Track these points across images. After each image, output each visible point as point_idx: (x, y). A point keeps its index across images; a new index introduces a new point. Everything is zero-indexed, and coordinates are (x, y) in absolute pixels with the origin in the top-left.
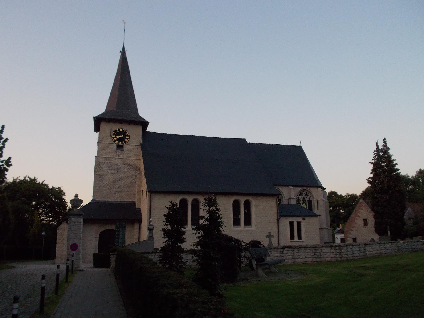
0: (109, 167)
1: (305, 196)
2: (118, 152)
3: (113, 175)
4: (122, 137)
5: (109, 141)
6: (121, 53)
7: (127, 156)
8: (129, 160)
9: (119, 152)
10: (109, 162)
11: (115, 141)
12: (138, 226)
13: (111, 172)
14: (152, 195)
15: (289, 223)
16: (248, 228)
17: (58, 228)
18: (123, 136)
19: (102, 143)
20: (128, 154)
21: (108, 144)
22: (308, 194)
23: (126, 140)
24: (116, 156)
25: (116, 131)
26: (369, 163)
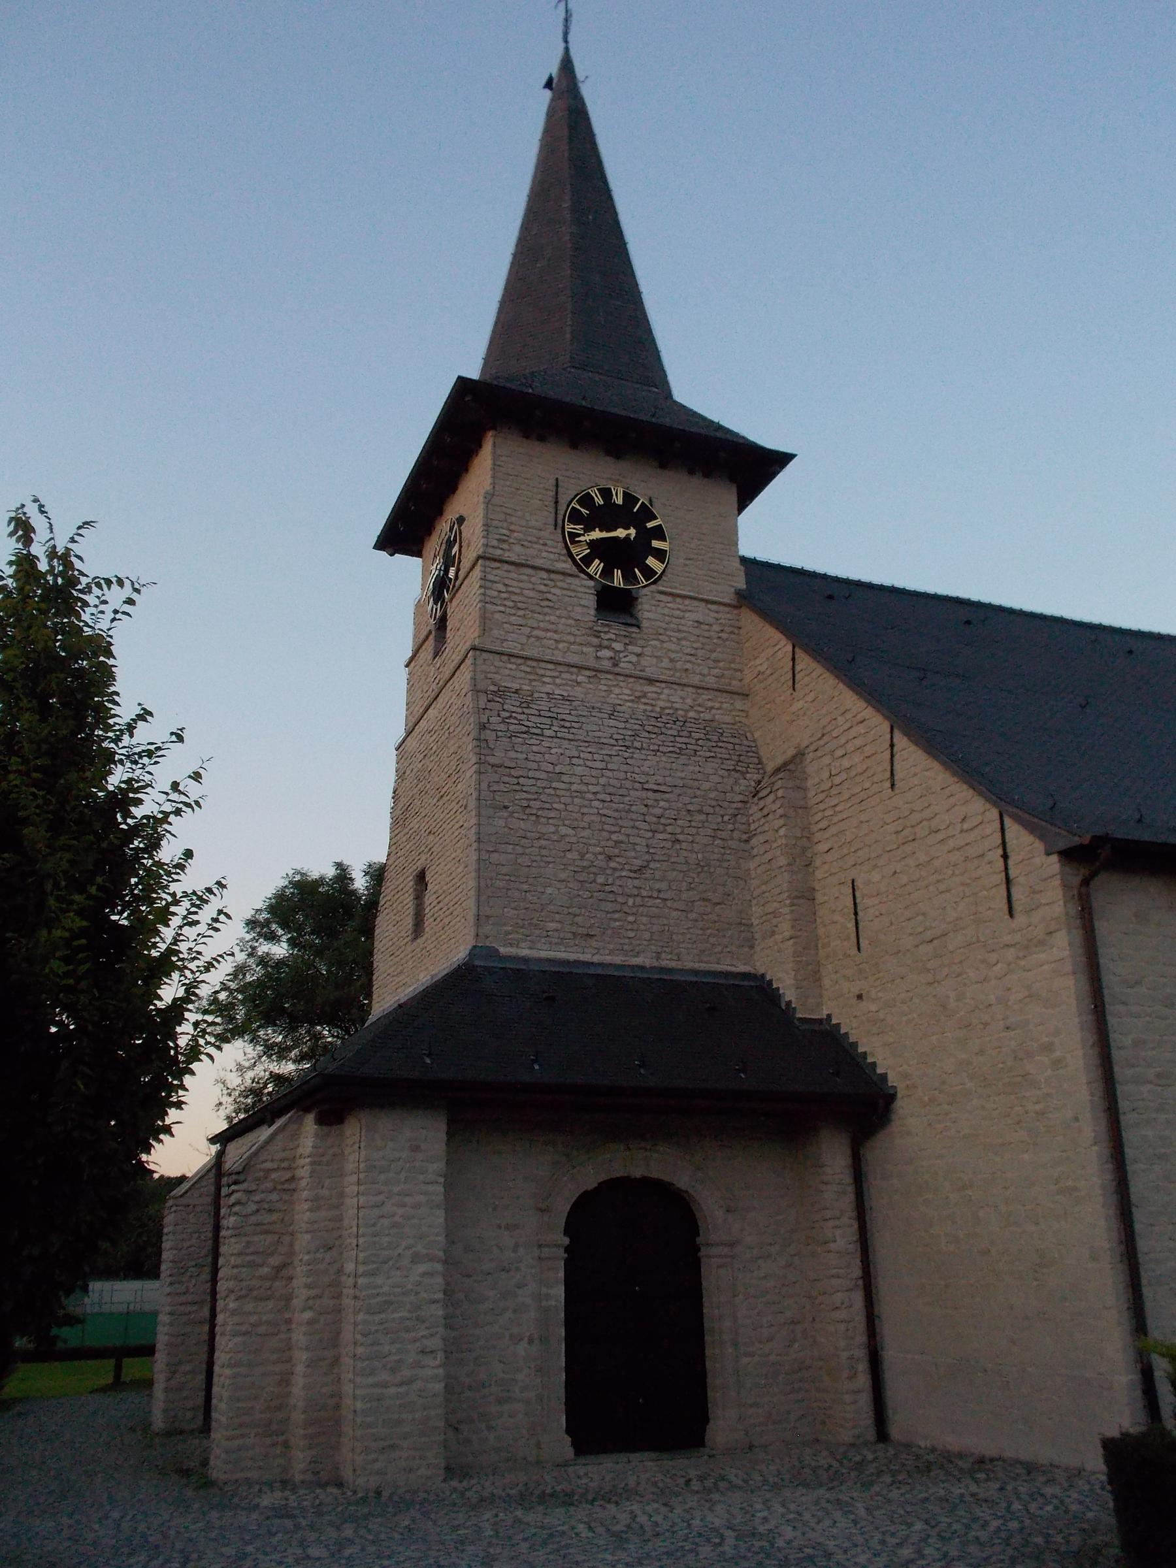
2: (606, 633)
3: (602, 781)
4: (628, 537)
5: (545, 554)
6: (548, 94)
7: (666, 663)
9: (613, 631)
11: (587, 560)
12: (849, 1152)
13: (589, 756)
14: (1099, 900)
18: (632, 532)
19: (506, 566)
20: (673, 655)
21: (544, 575)
23: (651, 561)
24: (597, 658)
25: (586, 500)
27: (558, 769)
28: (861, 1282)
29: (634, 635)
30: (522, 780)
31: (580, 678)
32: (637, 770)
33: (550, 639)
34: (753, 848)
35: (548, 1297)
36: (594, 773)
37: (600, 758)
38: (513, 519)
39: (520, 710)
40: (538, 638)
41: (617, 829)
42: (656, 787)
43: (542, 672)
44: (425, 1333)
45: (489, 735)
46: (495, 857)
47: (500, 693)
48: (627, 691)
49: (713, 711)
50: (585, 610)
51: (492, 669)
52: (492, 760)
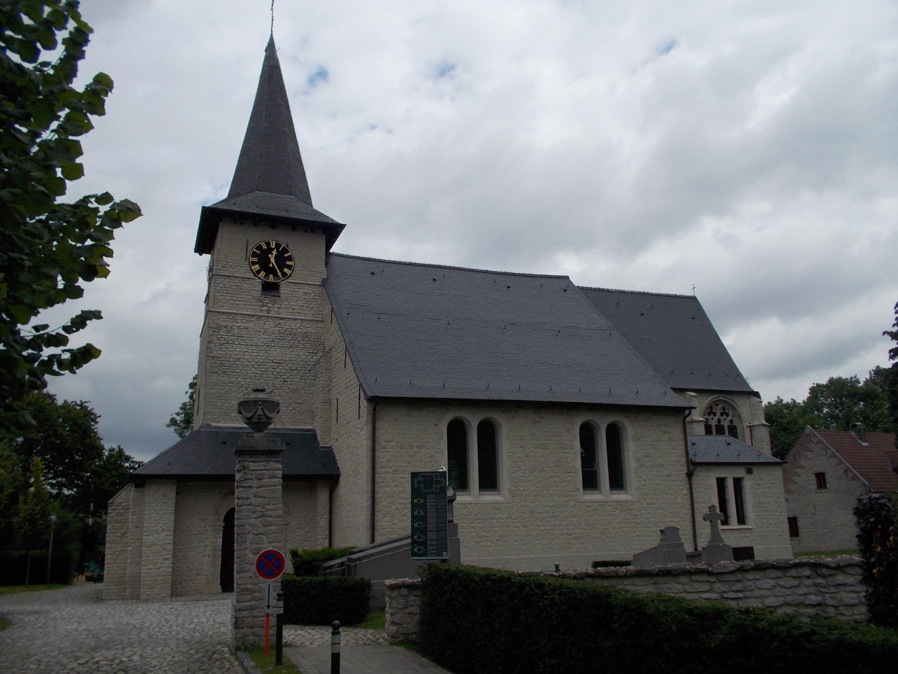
0: (245, 339)
1: (722, 416)
2: (265, 300)
8: (295, 322)
10: (243, 325)
15: (715, 481)
16: (489, 497)
17: (109, 502)
19: (224, 277)
20: (293, 307)
21: (240, 279)
22: (726, 411)
24: (261, 310)
26: (884, 333)
27: (238, 357)
28: (328, 536)
29: (277, 300)
30: (223, 362)
31: (253, 319)
32: (271, 355)
33: (241, 304)
34: (316, 382)
35: (216, 542)
36: (253, 357)
37: (256, 351)
38: (229, 257)
39: (226, 334)
40: (236, 304)
41: (261, 378)
42: (278, 362)
43: (237, 318)
44: (166, 553)
45: (211, 345)
46: (212, 391)
47: (219, 328)
48: (273, 323)
49: (309, 329)
50: (257, 292)
51: (216, 318)
52: (211, 355)
